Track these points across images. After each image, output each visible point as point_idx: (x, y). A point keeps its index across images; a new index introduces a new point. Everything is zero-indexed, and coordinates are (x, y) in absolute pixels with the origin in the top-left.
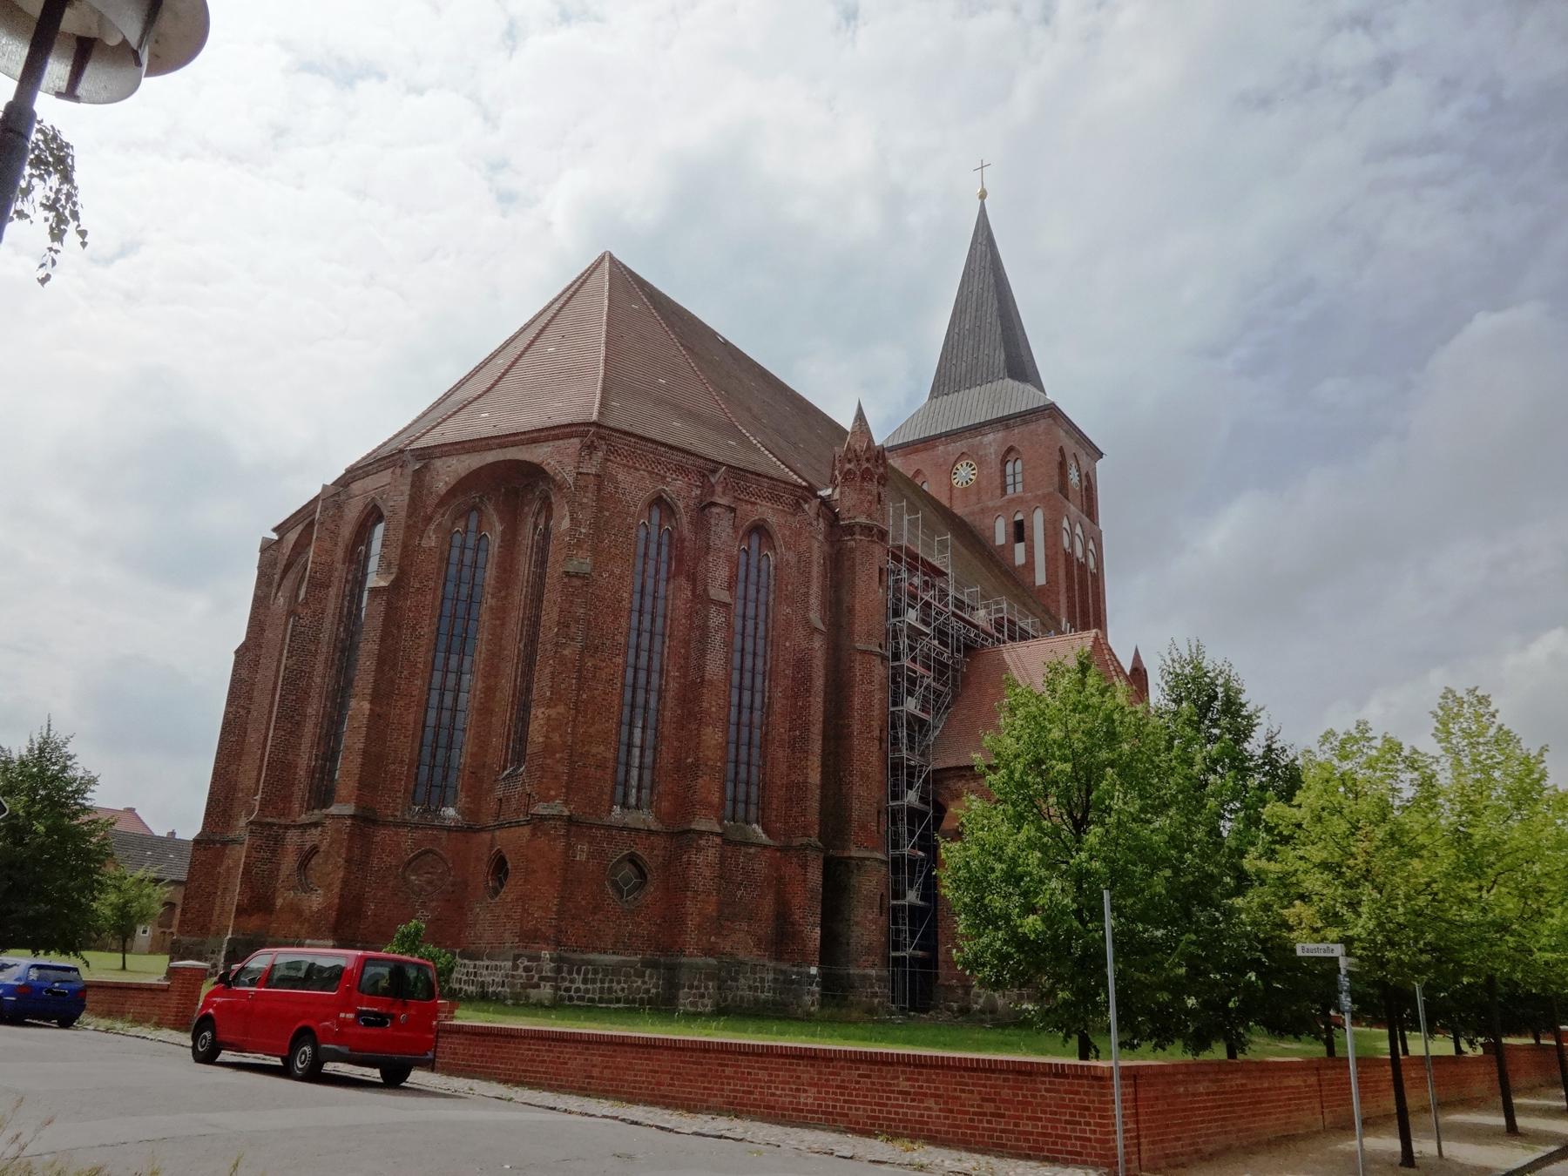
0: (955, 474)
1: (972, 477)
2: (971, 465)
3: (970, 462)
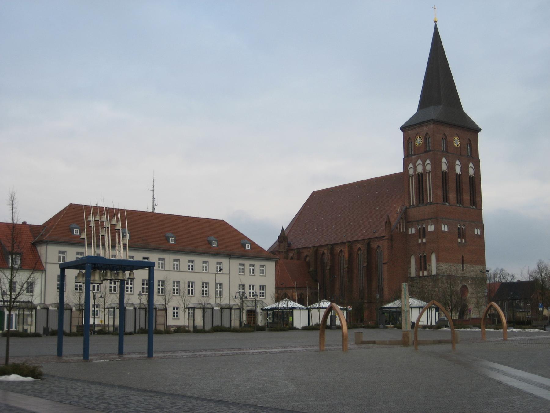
0: (416, 141)
1: (421, 142)
2: (421, 138)
3: (420, 137)
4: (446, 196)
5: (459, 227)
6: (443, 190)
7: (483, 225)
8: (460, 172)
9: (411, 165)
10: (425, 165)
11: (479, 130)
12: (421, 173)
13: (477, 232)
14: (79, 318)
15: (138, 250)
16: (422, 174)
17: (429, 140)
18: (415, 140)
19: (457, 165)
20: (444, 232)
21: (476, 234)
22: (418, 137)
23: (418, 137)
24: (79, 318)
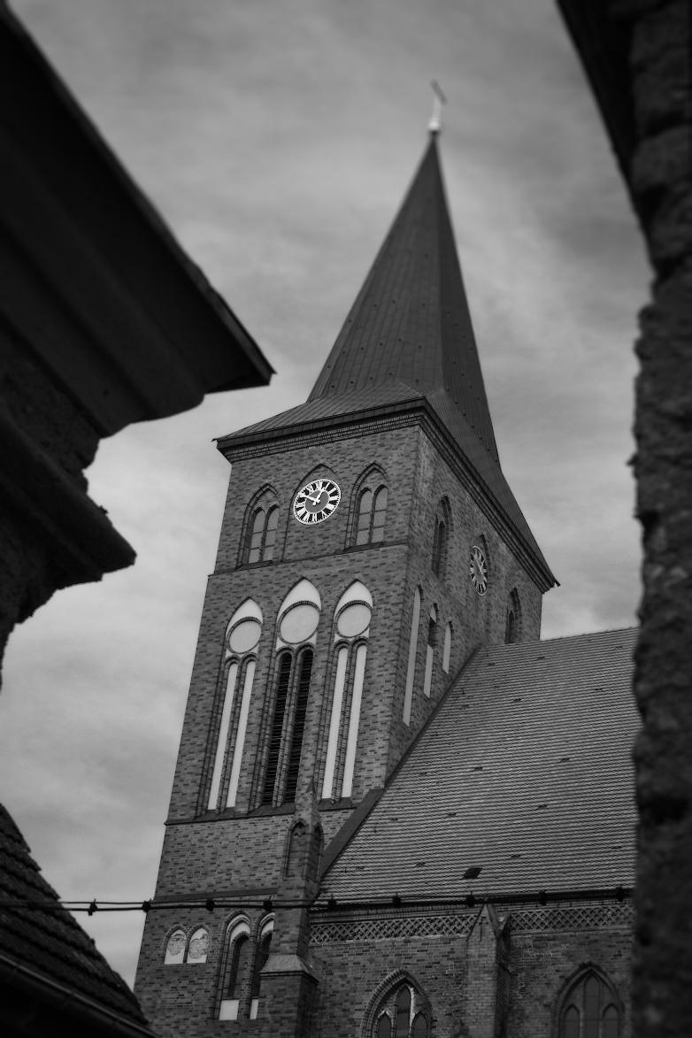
10: (281, 613)
12: (308, 645)
14: (371, 523)
16: (307, 653)
17: (268, 517)
18: (296, 491)
22: (319, 487)
24: (371, 523)
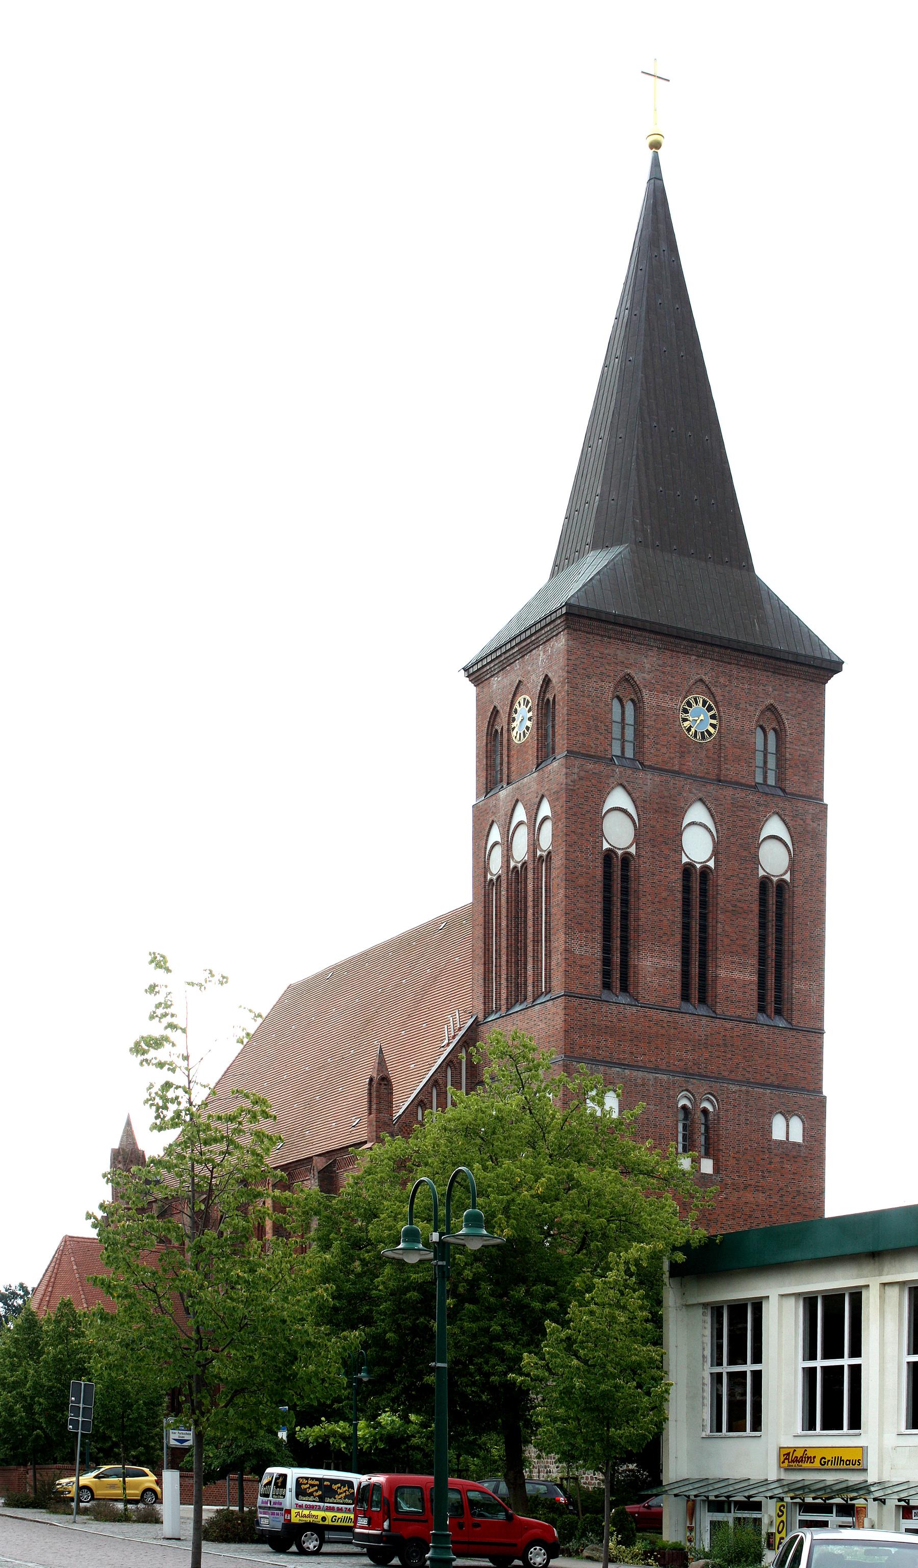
4: (625, 964)
5: (683, 1102)
6: (607, 936)
7: (822, 1102)
8: (708, 860)
9: (495, 835)
11: (833, 666)
13: (788, 1133)
15: (808, 1342)
19: (693, 823)
20: (786, 1145)
21: (782, 1137)
22: (712, 730)
23: (712, 730)
